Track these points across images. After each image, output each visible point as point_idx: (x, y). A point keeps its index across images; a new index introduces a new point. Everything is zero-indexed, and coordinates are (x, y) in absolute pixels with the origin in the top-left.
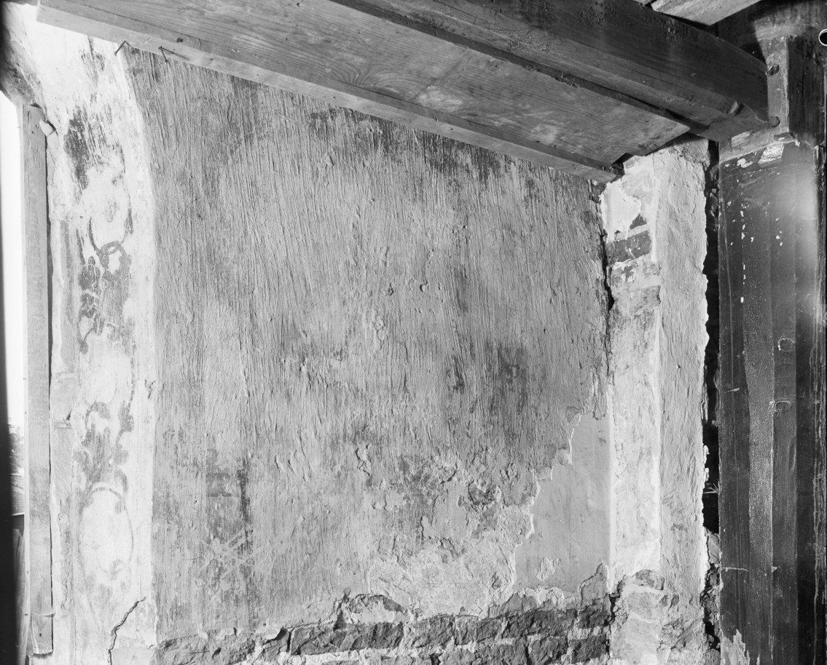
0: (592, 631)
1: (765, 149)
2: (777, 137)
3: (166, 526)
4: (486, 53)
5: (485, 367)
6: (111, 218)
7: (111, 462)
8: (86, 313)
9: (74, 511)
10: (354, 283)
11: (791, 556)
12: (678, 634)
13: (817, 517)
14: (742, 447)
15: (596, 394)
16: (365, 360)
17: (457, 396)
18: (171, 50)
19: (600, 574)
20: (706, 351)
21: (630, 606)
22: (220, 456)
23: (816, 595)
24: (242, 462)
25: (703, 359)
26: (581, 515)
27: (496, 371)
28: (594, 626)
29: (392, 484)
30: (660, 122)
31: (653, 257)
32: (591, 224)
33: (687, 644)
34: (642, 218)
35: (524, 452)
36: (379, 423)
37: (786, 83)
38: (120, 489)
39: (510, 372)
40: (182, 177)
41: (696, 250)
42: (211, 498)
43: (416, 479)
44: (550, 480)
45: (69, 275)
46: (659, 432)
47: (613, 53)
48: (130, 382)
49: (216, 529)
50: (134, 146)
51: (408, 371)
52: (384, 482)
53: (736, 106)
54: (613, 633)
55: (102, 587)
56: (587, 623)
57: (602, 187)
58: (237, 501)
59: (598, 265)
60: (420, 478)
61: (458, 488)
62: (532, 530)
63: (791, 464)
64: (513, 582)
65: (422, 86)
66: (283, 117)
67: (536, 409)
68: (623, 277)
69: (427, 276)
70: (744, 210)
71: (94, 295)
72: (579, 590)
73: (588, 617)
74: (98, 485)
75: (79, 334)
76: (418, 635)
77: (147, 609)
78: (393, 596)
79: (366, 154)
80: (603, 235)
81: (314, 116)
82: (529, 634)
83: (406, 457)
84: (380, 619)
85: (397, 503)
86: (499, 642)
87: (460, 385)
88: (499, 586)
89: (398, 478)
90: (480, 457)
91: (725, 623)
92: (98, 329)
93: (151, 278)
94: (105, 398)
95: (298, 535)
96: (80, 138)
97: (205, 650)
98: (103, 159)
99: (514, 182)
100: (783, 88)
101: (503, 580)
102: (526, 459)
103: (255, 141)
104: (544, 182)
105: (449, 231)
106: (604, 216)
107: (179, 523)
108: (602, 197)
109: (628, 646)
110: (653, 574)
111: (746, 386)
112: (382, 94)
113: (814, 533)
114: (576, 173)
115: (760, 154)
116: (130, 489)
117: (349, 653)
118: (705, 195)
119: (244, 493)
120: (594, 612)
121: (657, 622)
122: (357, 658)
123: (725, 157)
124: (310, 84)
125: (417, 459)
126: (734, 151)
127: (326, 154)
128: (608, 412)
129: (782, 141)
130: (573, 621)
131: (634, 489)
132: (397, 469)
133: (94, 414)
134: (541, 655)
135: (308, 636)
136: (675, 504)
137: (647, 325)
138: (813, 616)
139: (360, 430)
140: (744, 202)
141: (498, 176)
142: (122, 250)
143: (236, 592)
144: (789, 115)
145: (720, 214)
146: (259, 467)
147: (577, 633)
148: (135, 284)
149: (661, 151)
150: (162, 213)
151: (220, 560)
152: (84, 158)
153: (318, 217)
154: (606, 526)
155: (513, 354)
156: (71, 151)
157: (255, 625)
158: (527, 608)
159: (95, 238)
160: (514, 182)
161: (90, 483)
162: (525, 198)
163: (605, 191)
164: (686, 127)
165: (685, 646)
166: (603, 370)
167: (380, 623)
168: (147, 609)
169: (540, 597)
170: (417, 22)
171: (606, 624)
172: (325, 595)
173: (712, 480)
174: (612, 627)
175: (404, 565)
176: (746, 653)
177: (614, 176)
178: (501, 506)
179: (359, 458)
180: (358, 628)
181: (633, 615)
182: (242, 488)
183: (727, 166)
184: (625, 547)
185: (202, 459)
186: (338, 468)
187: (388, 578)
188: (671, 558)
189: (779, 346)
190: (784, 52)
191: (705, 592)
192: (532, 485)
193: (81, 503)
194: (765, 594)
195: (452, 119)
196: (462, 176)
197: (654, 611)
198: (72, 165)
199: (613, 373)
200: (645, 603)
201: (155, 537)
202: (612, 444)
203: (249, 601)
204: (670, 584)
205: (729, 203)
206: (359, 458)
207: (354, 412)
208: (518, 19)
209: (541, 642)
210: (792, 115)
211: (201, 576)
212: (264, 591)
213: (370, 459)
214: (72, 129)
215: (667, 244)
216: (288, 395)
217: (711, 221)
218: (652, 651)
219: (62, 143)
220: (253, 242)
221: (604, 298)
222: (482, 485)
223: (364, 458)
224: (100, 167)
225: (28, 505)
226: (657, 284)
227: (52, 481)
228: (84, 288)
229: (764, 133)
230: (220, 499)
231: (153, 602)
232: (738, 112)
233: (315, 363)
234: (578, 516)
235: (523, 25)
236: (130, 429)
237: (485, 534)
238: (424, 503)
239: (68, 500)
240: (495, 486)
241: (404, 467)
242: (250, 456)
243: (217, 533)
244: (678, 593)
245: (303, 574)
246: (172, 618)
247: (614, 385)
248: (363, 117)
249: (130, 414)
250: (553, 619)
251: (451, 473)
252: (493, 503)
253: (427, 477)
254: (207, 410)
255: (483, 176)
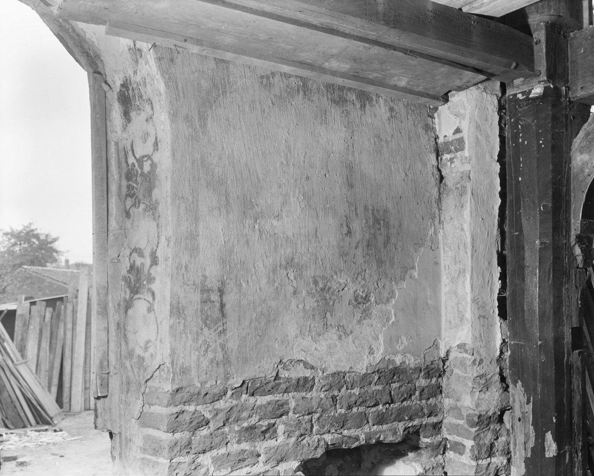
0: (431, 381)
1: (533, 89)
2: (539, 82)
3: (178, 321)
4: (363, 42)
5: (364, 221)
6: (145, 141)
7: (145, 283)
8: (130, 195)
9: (122, 311)
10: (286, 174)
11: (550, 335)
12: (483, 383)
13: (565, 311)
14: (521, 268)
15: (433, 235)
16: (292, 220)
17: (347, 239)
18: (181, 46)
19: (435, 345)
20: (499, 209)
21: (454, 365)
22: (208, 279)
23: (566, 358)
24: (221, 282)
25: (497, 214)
26: (423, 309)
27: (371, 223)
28: (432, 377)
29: (309, 293)
30: (468, 75)
31: (466, 153)
32: (429, 131)
33: (489, 389)
34: (459, 129)
35: (388, 272)
36: (301, 257)
37: (544, 51)
38: (150, 299)
39: (379, 224)
40: (187, 118)
41: (493, 148)
42: (203, 304)
43: (322, 290)
44: (404, 288)
45: (120, 173)
46: (470, 259)
47: (437, 39)
48: (156, 236)
49: (205, 322)
50: (159, 101)
51: (318, 225)
52: (304, 292)
53: (514, 64)
54: (444, 382)
55: (139, 356)
56: (428, 376)
57: (436, 109)
58: (218, 305)
59: (433, 157)
60: (325, 289)
61: (348, 294)
62: (393, 319)
63: (549, 279)
64: (382, 351)
65: (326, 59)
66: (244, 79)
67: (395, 245)
68: (449, 163)
69: (329, 168)
70: (521, 125)
71: (135, 185)
72: (422, 356)
73: (428, 372)
74: (137, 296)
75: (125, 207)
76: (324, 384)
77: (166, 369)
78: (309, 360)
79: (293, 98)
80: (437, 138)
81: (262, 77)
82: (392, 383)
83: (317, 276)
84: (301, 375)
85: (311, 305)
86: (374, 388)
87: (349, 233)
88: (373, 354)
89: (312, 289)
90: (362, 275)
91: (512, 375)
92: (137, 205)
93: (169, 177)
94: (142, 245)
95: (253, 325)
96: (127, 94)
97: (199, 394)
98: (141, 107)
99: (382, 110)
100: (543, 54)
101: (376, 350)
102: (389, 276)
103: (228, 95)
104: (400, 107)
105: (342, 141)
106: (437, 127)
107: (185, 319)
108: (436, 115)
109: (453, 390)
110: (468, 346)
111: (522, 231)
112: (302, 64)
113: (563, 321)
114: (420, 102)
115: (530, 92)
116: (157, 300)
117: (283, 395)
118: (498, 114)
119: (222, 301)
120: (432, 369)
121: (470, 375)
122: (288, 398)
123: (510, 92)
124: (260, 60)
125: (323, 278)
126: (515, 89)
127: (269, 99)
128: (440, 246)
129: (543, 84)
130: (419, 375)
131: (456, 293)
132: (312, 284)
133: (135, 255)
134: (400, 396)
135: (259, 385)
136: (480, 304)
137: (463, 194)
138: (564, 371)
139: (290, 262)
140: (521, 120)
141: (372, 106)
142: (152, 160)
143: (217, 359)
144: (547, 69)
145: (507, 126)
146: (231, 285)
147: (422, 382)
148: (160, 180)
149: (471, 88)
150: (176, 138)
151: (208, 340)
152: (129, 106)
153: (264, 136)
154: (439, 315)
155: (381, 213)
156: (121, 101)
157: (228, 379)
158: (391, 367)
159: (135, 152)
160: (382, 110)
161: (132, 295)
162: (388, 118)
163: (438, 111)
164: (484, 77)
165: (487, 390)
166: (437, 220)
167: (301, 377)
168: (166, 369)
169: (398, 360)
170: (323, 28)
171: (440, 376)
172: (268, 360)
173: (503, 288)
174: (443, 378)
175: (315, 342)
176: (524, 394)
177: (443, 103)
178: (374, 304)
179: (288, 278)
180: (288, 380)
181: (456, 371)
182: (221, 298)
183: (511, 97)
184: (451, 329)
185: (198, 281)
186: (276, 284)
187: (306, 350)
188: (478, 336)
189: (542, 208)
190: (543, 32)
191: (500, 356)
192: (393, 291)
193: (127, 306)
194: (537, 358)
195: (344, 75)
196: (350, 107)
197: (468, 368)
198: (121, 109)
199: (443, 222)
200: (462, 363)
201: (171, 327)
202: (442, 265)
203: (224, 364)
204: (478, 352)
205: (512, 120)
206: (288, 278)
207: (286, 251)
208: (381, 24)
209: (399, 388)
210: (548, 70)
211: (197, 350)
212: (233, 358)
213: (295, 278)
214: (122, 89)
215: (475, 145)
216: (247, 242)
217: (501, 130)
218: (467, 393)
219: (116, 97)
220: (227, 153)
221: (437, 176)
222: (363, 292)
223: (292, 278)
224: (139, 112)
225: (95, 307)
226: (468, 169)
227: (110, 293)
228: (128, 181)
229: (532, 79)
230: (208, 304)
231: (170, 366)
232: (516, 67)
233: (263, 222)
234: (421, 310)
235: (385, 27)
236: (157, 264)
237: (365, 322)
238: (327, 304)
239: (119, 305)
240: (370, 293)
241: (316, 283)
242: (225, 279)
243: (206, 324)
244: (483, 357)
245: (256, 348)
246: (180, 375)
247: (443, 229)
248: (290, 76)
249: (157, 255)
250: (407, 373)
251: (344, 285)
252: (369, 303)
253: (329, 288)
254: (201, 252)
255: (363, 107)
